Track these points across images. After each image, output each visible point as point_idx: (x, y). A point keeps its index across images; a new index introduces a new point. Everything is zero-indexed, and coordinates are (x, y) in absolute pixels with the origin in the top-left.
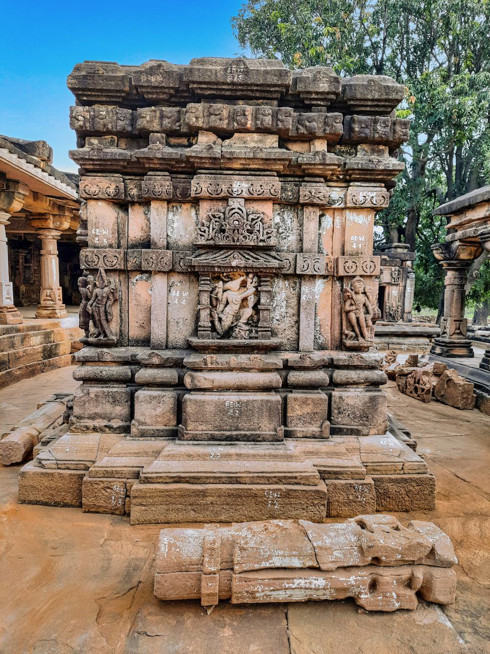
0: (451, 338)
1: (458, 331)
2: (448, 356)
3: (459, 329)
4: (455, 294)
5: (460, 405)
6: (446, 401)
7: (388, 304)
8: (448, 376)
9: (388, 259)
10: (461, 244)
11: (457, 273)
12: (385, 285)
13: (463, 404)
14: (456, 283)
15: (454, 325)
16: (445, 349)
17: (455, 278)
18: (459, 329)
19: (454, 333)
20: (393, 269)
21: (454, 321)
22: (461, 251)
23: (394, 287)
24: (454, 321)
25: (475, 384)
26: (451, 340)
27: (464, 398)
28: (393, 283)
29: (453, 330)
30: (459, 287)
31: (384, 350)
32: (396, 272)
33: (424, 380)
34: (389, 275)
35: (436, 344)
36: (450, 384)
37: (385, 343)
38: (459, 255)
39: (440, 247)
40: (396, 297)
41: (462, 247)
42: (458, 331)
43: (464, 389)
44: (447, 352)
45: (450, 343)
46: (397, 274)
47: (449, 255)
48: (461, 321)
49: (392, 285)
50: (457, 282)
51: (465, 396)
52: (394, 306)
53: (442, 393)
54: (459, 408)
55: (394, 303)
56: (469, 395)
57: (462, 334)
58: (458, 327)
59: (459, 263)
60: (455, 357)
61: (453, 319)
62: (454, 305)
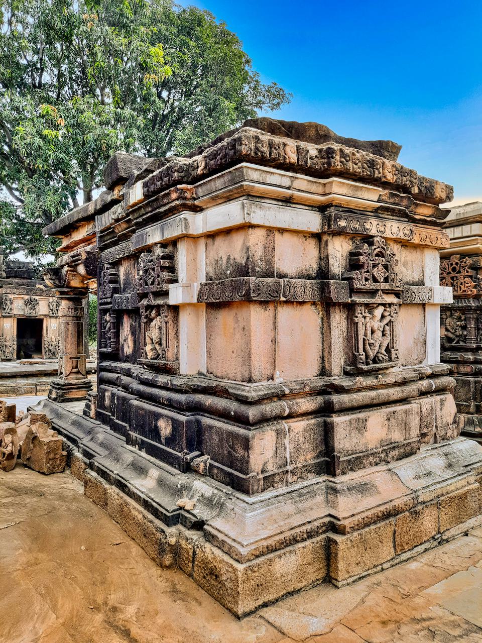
0: (67, 379)
1: (75, 370)
2: (63, 401)
3: (77, 367)
4: (70, 327)
5: (45, 470)
6: (33, 466)
7: (46, 339)
8: (33, 433)
9: (44, 288)
10: (70, 269)
11: (71, 303)
12: (42, 317)
13: (49, 468)
14: (70, 314)
15: (71, 363)
16: (60, 392)
17: (69, 309)
18: (77, 367)
19: (71, 373)
20: (51, 299)
21: (71, 358)
22: (71, 277)
23: (53, 320)
24: (71, 358)
25: (441, 307)
26: (67, 382)
27: (50, 459)
28: (51, 315)
29: (69, 370)
30: (75, 319)
31: (31, 392)
32: (54, 303)
33: (6, 442)
34: (46, 306)
35: (53, 387)
36: (36, 443)
37: (32, 384)
38: (69, 283)
39: (48, 272)
40: (55, 331)
41: (72, 273)
42: (75, 370)
43: (49, 447)
44: (62, 396)
45: (65, 385)
46: (55, 306)
47: (60, 282)
48: (79, 358)
49: (51, 317)
50: (71, 313)
51: (51, 456)
52: (54, 340)
53: (28, 455)
54: (44, 474)
55: (53, 337)
56: (56, 454)
57: (81, 373)
58: (75, 365)
59: (71, 291)
60: (72, 401)
61: (69, 356)
62: (69, 340)
